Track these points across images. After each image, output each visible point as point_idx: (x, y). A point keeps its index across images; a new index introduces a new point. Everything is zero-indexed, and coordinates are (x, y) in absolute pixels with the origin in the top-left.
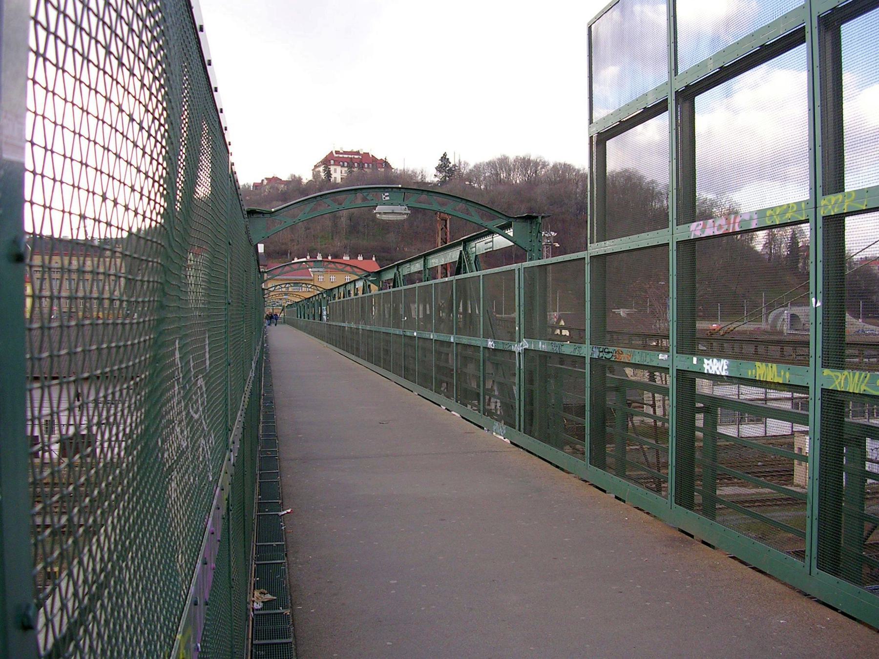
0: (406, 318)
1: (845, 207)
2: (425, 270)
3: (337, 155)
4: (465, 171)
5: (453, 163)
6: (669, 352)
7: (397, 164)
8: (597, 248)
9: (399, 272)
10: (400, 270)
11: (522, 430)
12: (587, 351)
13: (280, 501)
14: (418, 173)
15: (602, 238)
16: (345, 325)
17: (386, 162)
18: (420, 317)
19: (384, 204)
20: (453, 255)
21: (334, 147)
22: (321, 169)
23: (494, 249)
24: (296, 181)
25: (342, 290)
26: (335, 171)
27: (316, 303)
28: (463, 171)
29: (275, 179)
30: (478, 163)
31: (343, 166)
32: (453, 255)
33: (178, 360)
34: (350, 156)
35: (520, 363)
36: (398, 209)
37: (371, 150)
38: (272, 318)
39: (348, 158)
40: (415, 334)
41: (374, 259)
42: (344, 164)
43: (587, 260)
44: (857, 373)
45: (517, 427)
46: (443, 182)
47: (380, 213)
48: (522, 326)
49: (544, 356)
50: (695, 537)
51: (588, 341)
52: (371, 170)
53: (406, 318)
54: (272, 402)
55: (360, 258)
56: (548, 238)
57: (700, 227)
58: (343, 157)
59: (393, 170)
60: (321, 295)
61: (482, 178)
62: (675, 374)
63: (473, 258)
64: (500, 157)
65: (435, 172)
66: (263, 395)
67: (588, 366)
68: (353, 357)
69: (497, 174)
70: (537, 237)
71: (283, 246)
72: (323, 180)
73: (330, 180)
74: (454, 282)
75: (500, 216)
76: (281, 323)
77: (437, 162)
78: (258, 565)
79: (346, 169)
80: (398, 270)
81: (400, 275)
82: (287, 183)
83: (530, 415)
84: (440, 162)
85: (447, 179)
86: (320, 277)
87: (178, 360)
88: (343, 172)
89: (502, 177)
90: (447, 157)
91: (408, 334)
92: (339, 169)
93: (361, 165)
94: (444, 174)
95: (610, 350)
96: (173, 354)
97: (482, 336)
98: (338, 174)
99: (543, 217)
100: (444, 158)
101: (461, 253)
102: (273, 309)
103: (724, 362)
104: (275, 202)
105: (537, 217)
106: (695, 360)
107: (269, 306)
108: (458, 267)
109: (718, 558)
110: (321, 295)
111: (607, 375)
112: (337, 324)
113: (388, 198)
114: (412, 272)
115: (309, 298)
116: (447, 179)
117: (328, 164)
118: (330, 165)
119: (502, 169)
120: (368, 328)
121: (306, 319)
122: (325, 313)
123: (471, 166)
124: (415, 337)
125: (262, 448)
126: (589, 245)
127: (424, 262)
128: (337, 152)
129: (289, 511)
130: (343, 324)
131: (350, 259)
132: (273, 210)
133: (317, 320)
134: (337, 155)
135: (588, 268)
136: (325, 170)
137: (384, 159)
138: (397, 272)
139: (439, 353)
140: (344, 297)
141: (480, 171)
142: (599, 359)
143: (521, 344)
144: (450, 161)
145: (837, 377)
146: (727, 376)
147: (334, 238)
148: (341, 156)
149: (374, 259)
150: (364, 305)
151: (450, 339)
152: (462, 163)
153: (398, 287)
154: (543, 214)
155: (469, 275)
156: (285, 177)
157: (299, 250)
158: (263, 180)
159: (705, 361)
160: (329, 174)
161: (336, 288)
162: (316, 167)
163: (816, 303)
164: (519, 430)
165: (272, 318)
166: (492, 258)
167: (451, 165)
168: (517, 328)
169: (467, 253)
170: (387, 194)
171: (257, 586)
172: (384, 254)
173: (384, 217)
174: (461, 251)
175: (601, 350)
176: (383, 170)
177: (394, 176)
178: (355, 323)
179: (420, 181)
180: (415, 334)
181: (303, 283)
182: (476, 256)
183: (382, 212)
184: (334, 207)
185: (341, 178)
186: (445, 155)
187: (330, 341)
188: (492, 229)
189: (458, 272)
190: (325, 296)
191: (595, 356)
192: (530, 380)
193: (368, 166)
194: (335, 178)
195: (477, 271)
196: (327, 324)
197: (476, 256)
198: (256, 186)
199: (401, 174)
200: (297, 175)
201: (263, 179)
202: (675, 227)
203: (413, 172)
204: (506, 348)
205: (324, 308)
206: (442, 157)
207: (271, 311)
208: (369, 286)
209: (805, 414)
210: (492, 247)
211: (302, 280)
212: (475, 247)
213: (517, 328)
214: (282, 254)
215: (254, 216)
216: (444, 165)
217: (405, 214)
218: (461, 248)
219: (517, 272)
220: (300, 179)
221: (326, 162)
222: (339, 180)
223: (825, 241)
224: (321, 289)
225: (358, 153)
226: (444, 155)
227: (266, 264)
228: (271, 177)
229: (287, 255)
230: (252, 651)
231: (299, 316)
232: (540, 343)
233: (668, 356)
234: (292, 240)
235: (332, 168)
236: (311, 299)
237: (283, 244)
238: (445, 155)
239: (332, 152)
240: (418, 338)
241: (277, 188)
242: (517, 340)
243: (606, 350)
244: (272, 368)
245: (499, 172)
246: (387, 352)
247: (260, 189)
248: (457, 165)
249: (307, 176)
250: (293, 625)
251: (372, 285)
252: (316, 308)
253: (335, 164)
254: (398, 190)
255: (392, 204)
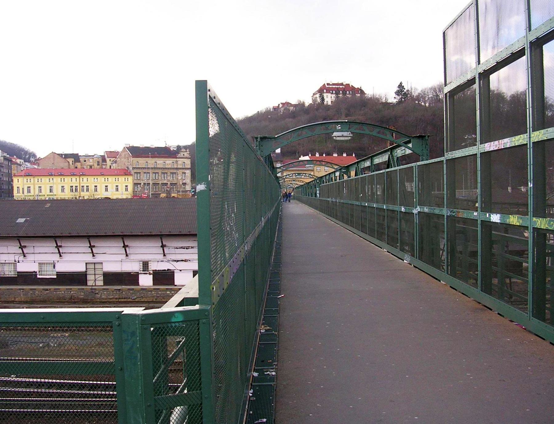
0: (361, 195)
1: (540, 138)
2: (372, 165)
3: (328, 86)
4: (415, 94)
5: (406, 89)
6: (477, 211)
7: (369, 91)
8: (450, 155)
9: (358, 167)
10: (359, 165)
11: (418, 258)
12: (445, 212)
13: (279, 292)
14: (383, 97)
15: (453, 149)
16: (329, 199)
17: (361, 90)
18: (369, 194)
19: (338, 131)
20: (385, 158)
21: (326, 81)
22: (318, 95)
23: (406, 154)
24: (300, 106)
25: (327, 177)
26: (327, 97)
27: (313, 185)
28: (413, 94)
29: (288, 104)
30: (424, 88)
31: (332, 93)
32: (385, 158)
33: (226, 207)
34: (337, 87)
35: (416, 220)
36: (345, 134)
37: (351, 82)
38: (287, 196)
39: (336, 87)
40: (366, 204)
41: (354, 155)
42: (333, 92)
43: (445, 162)
44: (544, 219)
45: (415, 257)
46: (400, 102)
47: (335, 137)
48: (417, 199)
49: (428, 215)
50: (505, 317)
51: (445, 206)
52: (351, 96)
53: (361, 195)
54: (280, 246)
55: (345, 155)
56: (470, 139)
57: (489, 145)
58: (332, 87)
59: (366, 95)
60: (315, 181)
61: (426, 99)
62: (532, 231)
63: (395, 159)
64: (439, 84)
65: (394, 95)
66: (276, 242)
67: (479, 226)
68: (334, 220)
69: (437, 96)
70: (425, 148)
71: (294, 148)
72: (319, 103)
73: (324, 103)
74: (385, 173)
75: (404, 136)
76: (292, 199)
77: (396, 89)
78: (264, 317)
79: (334, 95)
80: (357, 165)
81: (359, 169)
82: (295, 106)
83: (421, 250)
84: (398, 88)
85: (403, 100)
86: (318, 168)
87: (226, 207)
88: (332, 97)
89: (440, 97)
90: (402, 85)
91: (363, 204)
92: (329, 95)
93: (344, 93)
94: (401, 96)
95: (455, 211)
96: (225, 205)
97: (399, 205)
98: (329, 99)
99: (428, 136)
100: (401, 86)
101: (389, 156)
102: (287, 190)
103: (499, 215)
104: (287, 119)
105: (425, 136)
106: (488, 214)
107: (284, 188)
108: (388, 164)
109: (494, 316)
110: (315, 181)
111: (493, 232)
112: (325, 199)
113: (340, 128)
114: (365, 166)
115: (309, 183)
116: (403, 100)
117: (322, 92)
118: (324, 93)
119: (440, 92)
120: (342, 201)
121: (307, 196)
122: (318, 192)
123: (419, 91)
124: (366, 206)
125: (272, 268)
126: (445, 153)
127: (371, 161)
128: (328, 84)
129: (283, 295)
130: (328, 199)
131: (338, 155)
132: (276, 136)
133: (314, 197)
134: (328, 86)
135: (445, 166)
136: (320, 97)
137: (359, 88)
138: (357, 167)
139: (379, 215)
140: (329, 182)
141: (425, 94)
142: (450, 216)
143: (417, 209)
144: (405, 87)
145: (538, 221)
146: (500, 223)
147: (327, 142)
148: (331, 86)
149: (354, 155)
150: (339, 186)
151: (384, 207)
152: (413, 89)
153: (358, 176)
154: (429, 135)
155: (393, 169)
156: (294, 102)
157: (303, 150)
158: (279, 105)
159: (491, 215)
160: (323, 99)
161: (324, 176)
162: (314, 94)
163: (530, 185)
164: (416, 258)
165: (287, 196)
166: (405, 159)
167: (405, 91)
168: (415, 200)
169: (393, 156)
170: (339, 126)
171: (263, 324)
172: (361, 152)
173: (338, 138)
174: (389, 155)
175: (451, 211)
176: (359, 95)
177: (367, 99)
178: (335, 198)
179: (384, 102)
180: (366, 204)
181: (303, 174)
182: (397, 158)
183: (337, 136)
184: (310, 134)
185: (331, 102)
186: (401, 83)
187: (321, 211)
188: (400, 144)
189: (388, 168)
190: (318, 181)
191: (448, 214)
192: (421, 230)
193: (349, 93)
194: (327, 101)
195: (398, 166)
196: (319, 199)
197: (397, 158)
198: (274, 108)
199: (371, 98)
200: (302, 101)
201: (279, 103)
202: (479, 145)
203: (379, 96)
204: (410, 211)
205: (318, 189)
206: (399, 85)
207: (286, 191)
208: (343, 175)
209: (526, 240)
210: (405, 153)
211: (302, 170)
212: (397, 152)
213: (415, 200)
214: (293, 154)
215: (266, 140)
216: (401, 90)
217: (349, 136)
218: (389, 153)
219: (414, 168)
220: (303, 104)
221: (321, 91)
222: (330, 103)
223: (114, 200)
224: (315, 177)
225: (342, 84)
226: (400, 83)
227: (282, 160)
228: (284, 102)
229: (296, 154)
230: (258, 346)
231: (303, 194)
232: (425, 208)
233: (478, 213)
234: (299, 144)
235: (325, 95)
236: (310, 183)
237: (293, 147)
238: (401, 83)
239: (324, 84)
240: (387, 210)
241: (288, 109)
242: (415, 207)
243: (453, 211)
244: (283, 227)
245: (438, 94)
246: (352, 216)
247: (278, 110)
248: (410, 90)
249: (308, 101)
250: (278, 337)
251: (344, 175)
252: (313, 189)
253: (327, 92)
254: (346, 123)
255: (342, 131)
